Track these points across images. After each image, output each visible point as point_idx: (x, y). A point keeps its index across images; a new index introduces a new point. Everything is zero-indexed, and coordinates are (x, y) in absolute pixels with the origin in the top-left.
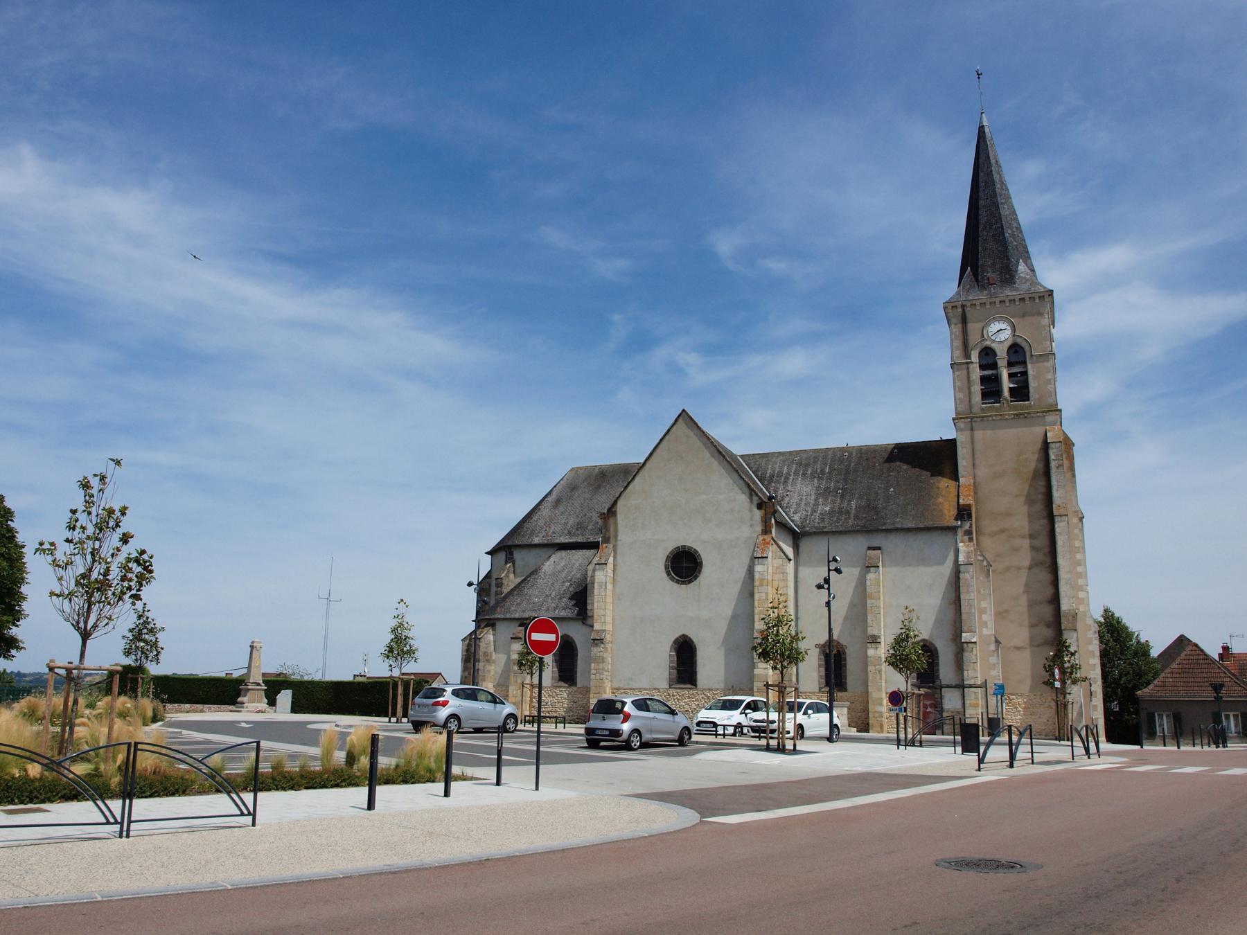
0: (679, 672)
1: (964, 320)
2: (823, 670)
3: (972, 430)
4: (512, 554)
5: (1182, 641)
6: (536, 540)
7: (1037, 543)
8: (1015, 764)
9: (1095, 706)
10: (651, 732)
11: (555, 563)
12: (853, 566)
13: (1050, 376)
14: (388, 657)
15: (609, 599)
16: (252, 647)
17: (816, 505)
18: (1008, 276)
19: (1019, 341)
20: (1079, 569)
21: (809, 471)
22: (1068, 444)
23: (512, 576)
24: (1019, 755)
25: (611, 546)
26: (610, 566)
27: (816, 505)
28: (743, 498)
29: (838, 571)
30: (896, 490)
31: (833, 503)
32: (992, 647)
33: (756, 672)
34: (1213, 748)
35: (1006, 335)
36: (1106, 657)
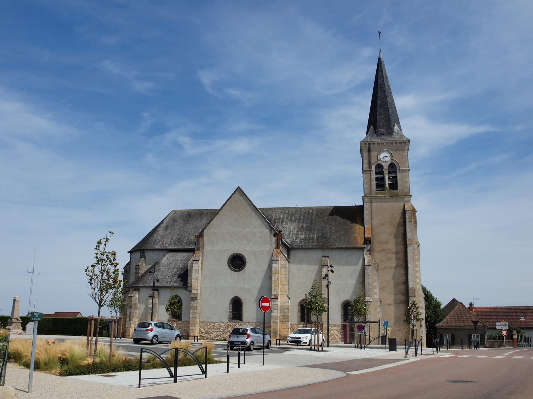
0: (233, 314)
1: (369, 151)
2: (300, 313)
3: (371, 202)
4: (144, 253)
5: (454, 301)
6: (157, 247)
7: (399, 256)
8: (417, 355)
9: (422, 331)
10: (257, 342)
11: (167, 259)
12: (315, 265)
13: (407, 179)
14: (110, 307)
15: (200, 278)
16: (15, 300)
17: (298, 234)
18: (390, 131)
19: (394, 162)
20: (417, 269)
21: (293, 218)
22: (414, 211)
23: (144, 264)
24: (418, 352)
25: (200, 252)
26: (200, 262)
27: (298, 234)
28: (267, 231)
29: (332, 271)
30: (332, 229)
31: (306, 234)
32: (379, 304)
33: (272, 314)
34: (469, 349)
35: (388, 159)
36: (427, 308)
